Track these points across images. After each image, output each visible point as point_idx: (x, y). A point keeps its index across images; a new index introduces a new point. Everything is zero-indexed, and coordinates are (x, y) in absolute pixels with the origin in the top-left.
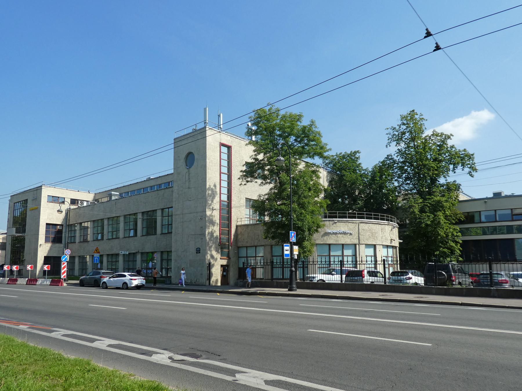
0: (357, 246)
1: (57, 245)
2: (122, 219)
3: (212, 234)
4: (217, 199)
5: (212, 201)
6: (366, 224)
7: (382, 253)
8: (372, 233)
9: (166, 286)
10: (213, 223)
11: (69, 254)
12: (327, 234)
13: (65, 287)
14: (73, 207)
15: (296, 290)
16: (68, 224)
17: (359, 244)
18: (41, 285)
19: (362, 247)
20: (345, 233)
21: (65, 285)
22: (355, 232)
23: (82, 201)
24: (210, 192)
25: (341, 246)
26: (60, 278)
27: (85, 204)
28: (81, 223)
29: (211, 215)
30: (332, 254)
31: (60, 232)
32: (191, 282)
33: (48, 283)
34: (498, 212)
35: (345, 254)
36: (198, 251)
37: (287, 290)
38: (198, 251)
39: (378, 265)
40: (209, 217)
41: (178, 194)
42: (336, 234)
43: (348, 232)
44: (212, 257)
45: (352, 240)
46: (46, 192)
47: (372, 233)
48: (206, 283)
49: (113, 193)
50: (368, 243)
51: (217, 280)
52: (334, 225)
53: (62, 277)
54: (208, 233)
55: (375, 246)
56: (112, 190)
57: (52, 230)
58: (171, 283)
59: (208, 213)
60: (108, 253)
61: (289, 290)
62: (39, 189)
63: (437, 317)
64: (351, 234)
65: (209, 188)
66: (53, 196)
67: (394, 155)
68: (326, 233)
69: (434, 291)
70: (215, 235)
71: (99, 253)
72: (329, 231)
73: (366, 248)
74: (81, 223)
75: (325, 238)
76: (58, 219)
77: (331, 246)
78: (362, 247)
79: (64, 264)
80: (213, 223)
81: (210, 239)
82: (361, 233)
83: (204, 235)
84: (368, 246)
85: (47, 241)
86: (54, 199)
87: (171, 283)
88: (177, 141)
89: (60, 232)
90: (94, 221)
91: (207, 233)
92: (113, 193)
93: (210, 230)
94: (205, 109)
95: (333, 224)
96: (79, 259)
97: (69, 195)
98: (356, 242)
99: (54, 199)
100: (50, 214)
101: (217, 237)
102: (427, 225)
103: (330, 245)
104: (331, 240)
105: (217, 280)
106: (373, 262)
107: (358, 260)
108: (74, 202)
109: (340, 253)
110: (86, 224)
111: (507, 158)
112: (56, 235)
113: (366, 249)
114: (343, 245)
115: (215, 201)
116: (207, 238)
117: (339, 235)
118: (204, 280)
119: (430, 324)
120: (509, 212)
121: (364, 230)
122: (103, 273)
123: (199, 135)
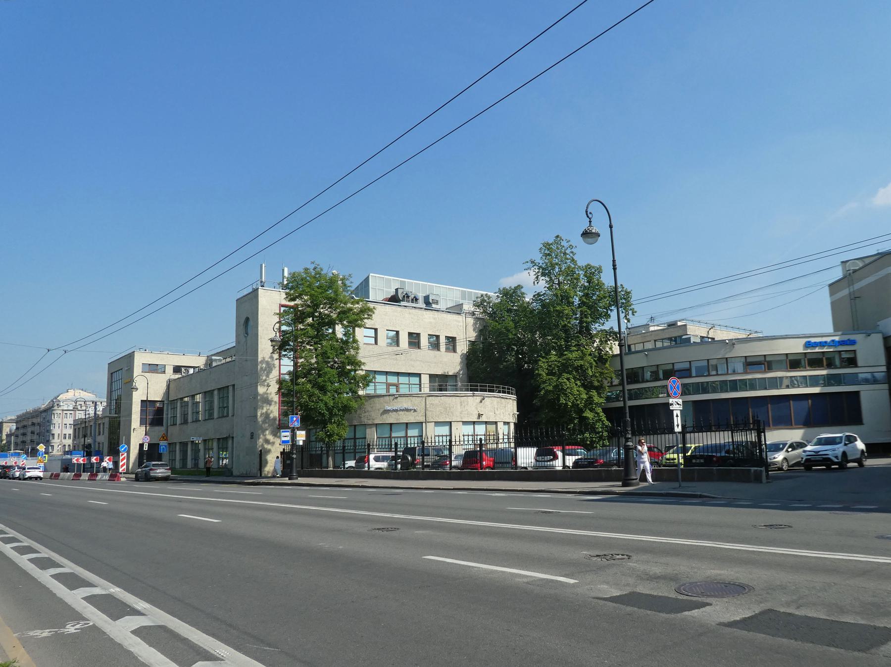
1: (157, 428)
3: (267, 416)
4: (275, 374)
5: (268, 376)
7: (502, 429)
10: (269, 402)
12: (386, 412)
16: (169, 400)
18: (100, 480)
19: (431, 426)
20: (407, 410)
21: (123, 479)
23: (187, 367)
24: (264, 366)
27: (191, 371)
28: (182, 399)
29: (266, 393)
31: (160, 411)
33: (107, 477)
34: (694, 365)
37: (620, 483)
40: (262, 395)
42: (396, 411)
44: (267, 441)
46: (140, 359)
49: (213, 358)
54: (262, 414)
55: (496, 423)
57: (151, 409)
59: (261, 390)
61: (623, 486)
62: (130, 357)
64: (415, 411)
67: (271, 357)
70: (272, 416)
75: (384, 416)
76: (157, 393)
77: (393, 427)
78: (431, 426)
80: (269, 402)
81: (264, 422)
83: (256, 416)
85: (143, 422)
86: (153, 368)
89: (160, 411)
90: (205, 392)
91: (259, 414)
93: (264, 410)
97: (171, 360)
98: (422, 419)
99: (153, 368)
100: (149, 387)
101: (274, 419)
102: (547, 392)
103: (391, 424)
104: (391, 419)
107: (453, 440)
108: (177, 369)
109: (402, 434)
110: (186, 399)
111: (763, 270)
112: (155, 414)
115: (271, 376)
116: (260, 420)
117: (401, 413)
118: (255, 470)
119: (402, 516)
120: (705, 363)
122: (154, 465)
123: (253, 296)
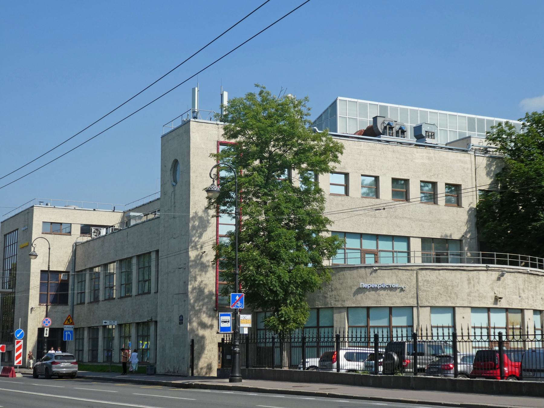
0: (415, 310)
1: (60, 308)
2: (134, 261)
3: (200, 290)
6: (432, 272)
8: (446, 288)
9: (107, 376)
11: (49, 325)
12: (361, 290)
13: (19, 380)
14: (86, 238)
15: (240, 381)
16: (76, 271)
17: (417, 307)
19: (425, 313)
20: (391, 288)
21: (18, 375)
22: (410, 287)
24: (197, 223)
25: (387, 311)
26: (13, 365)
27: (103, 232)
28: (91, 269)
30: (372, 323)
31: (64, 286)
32: (174, 372)
35: (394, 324)
36: (181, 320)
38: (181, 320)
39: (458, 343)
41: (164, 226)
42: (375, 289)
43: (397, 286)
45: (405, 300)
46: (40, 216)
47: (446, 288)
48: (188, 372)
50: (437, 305)
51: (209, 368)
52: (374, 274)
53: (16, 362)
54: (194, 289)
55: (522, 311)
56: (130, 211)
57: (53, 282)
58: (154, 373)
60: (137, 321)
61: (230, 381)
63: (192, 402)
64: (402, 290)
65: (193, 217)
66: (52, 223)
68: (360, 288)
69: (371, 381)
70: (206, 291)
71: (72, 323)
72: (365, 286)
73: (431, 312)
74: (91, 269)
75: (359, 297)
76: (60, 261)
77: (371, 311)
78: (425, 313)
79: (18, 342)
81: (197, 300)
82: (422, 288)
84: (435, 309)
87: (154, 373)
88: (163, 137)
89: (64, 285)
90: (121, 261)
91: (190, 290)
92: (132, 214)
94: (194, 90)
95: (371, 274)
96: (89, 333)
97: (78, 218)
98: (412, 302)
103: (368, 308)
105: (209, 368)
106: (451, 338)
108: (86, 229)
109: (384, 322)
110: (97, 270)
112: (58, 288)
113: (432, 315)
114: (391, 308)
116: (192, 298)
117: (382, 292)
118: (185, 368)
121: (427, 281)
123: (184, 130)
